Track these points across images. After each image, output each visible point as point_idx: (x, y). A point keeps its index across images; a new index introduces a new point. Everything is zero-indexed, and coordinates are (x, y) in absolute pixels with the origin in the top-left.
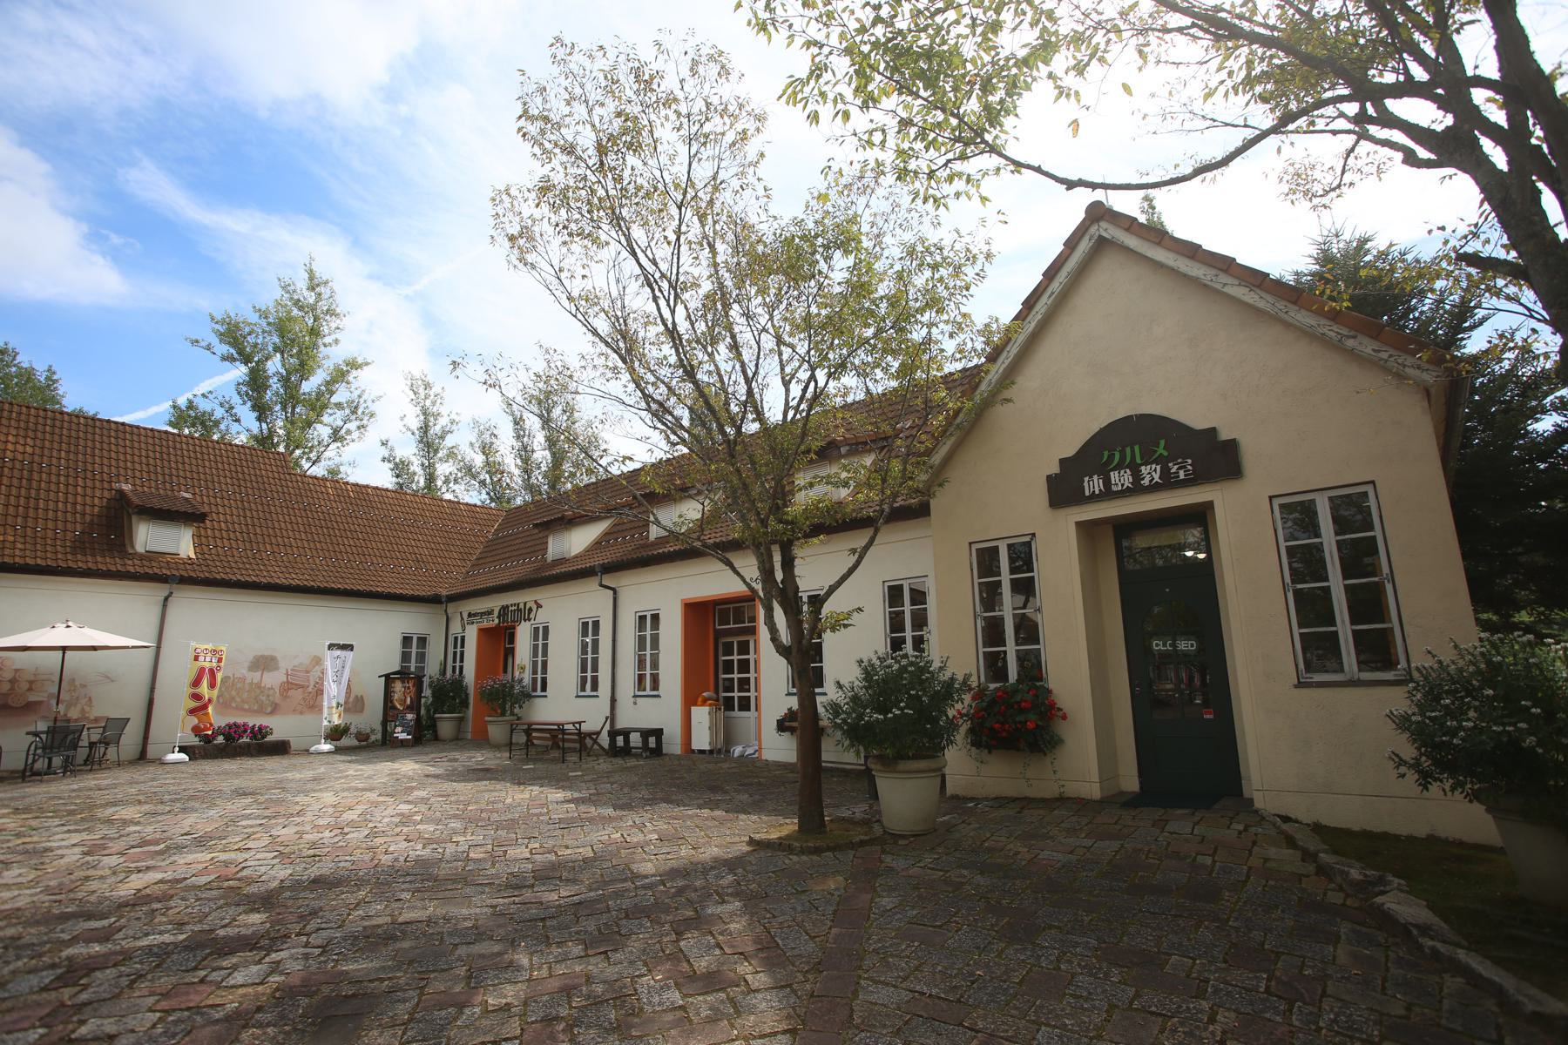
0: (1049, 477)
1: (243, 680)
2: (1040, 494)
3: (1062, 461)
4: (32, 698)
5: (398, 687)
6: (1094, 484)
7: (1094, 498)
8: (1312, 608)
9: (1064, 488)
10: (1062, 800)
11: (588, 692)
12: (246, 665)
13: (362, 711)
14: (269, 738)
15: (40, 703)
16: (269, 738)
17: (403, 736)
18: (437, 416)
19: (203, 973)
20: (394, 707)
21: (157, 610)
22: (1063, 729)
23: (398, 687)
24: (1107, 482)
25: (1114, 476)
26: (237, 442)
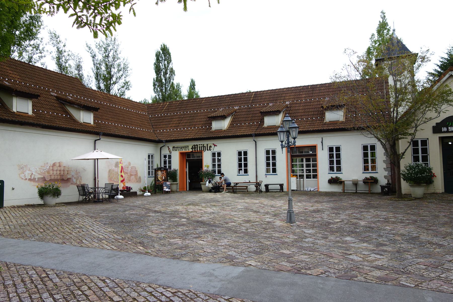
0: (433, 127)
1: (114, 170)
2: (431, 130)
3: (437, 123)
4: (69, 177)
5: (159, 173)
6: (444, 129)
7: (444, 132)
8: (425, 151)
9: (437, 129)
10: (434, 193)
11: (242, 172)
12: (114, 165)
13: (140, 182)
14: (131, 191)
15: (70, 178)
16: (131, 191)
17: (167, 190)
18: (118, 59)
19: (226, 251)
20: (159, 180)
21: (94, 143)
22: (434, 179)
23: (159, 173)
24: (448, 129)
25: (449, 128)
26: (36, 65)
